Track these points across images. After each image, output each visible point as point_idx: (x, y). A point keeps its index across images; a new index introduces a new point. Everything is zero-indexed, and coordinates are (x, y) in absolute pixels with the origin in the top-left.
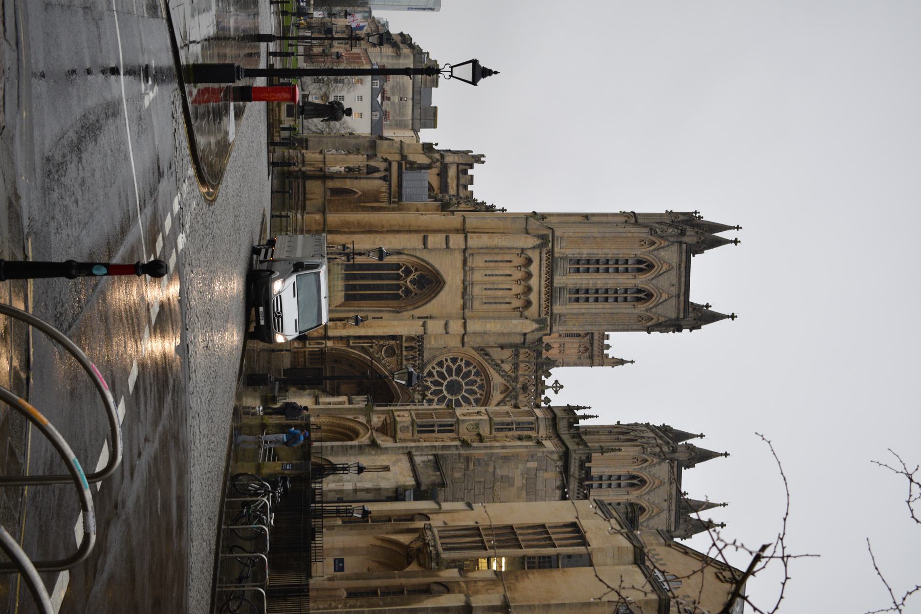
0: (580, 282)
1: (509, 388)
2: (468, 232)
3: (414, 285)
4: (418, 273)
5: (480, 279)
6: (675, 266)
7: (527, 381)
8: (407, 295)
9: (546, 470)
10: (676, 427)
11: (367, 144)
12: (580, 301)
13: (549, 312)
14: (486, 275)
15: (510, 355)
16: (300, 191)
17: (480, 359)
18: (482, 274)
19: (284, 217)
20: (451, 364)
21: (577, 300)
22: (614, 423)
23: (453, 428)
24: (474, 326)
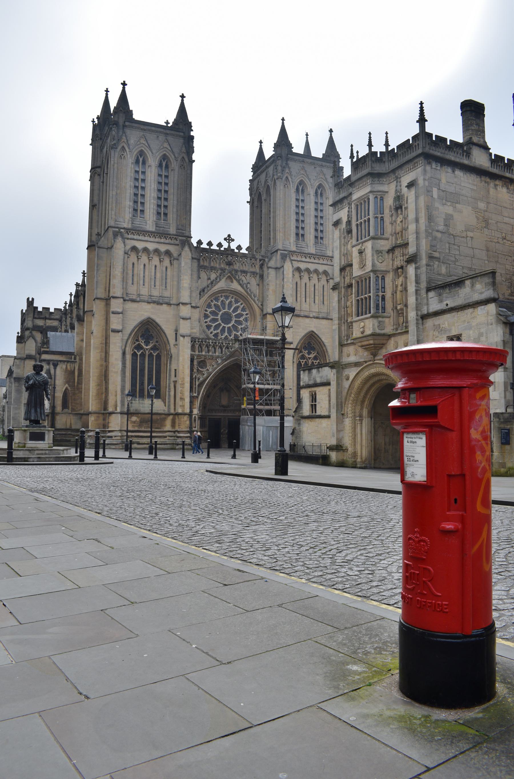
0: (152, 210)
1: (229, 276)
2: (109, 296)
3: (149, 342)
4: (140, 339)
5: (147, 289)
6: (142, 133)
7: (224, 262)
8: (158, 349)
9: (440, 180)
10: (253, 160)
11: (17, 384)
12: (167, 212)
13: (175, 237)
14: (144, 285)
15: (204, 273)
16: (64, 433)
17: (206, 296)
18: (143, 287)
19: (156, 446)
20: (209, 319)
21: (166, 214)
22: (248, 206)
23: (380, 276)
24: (185, 297)
